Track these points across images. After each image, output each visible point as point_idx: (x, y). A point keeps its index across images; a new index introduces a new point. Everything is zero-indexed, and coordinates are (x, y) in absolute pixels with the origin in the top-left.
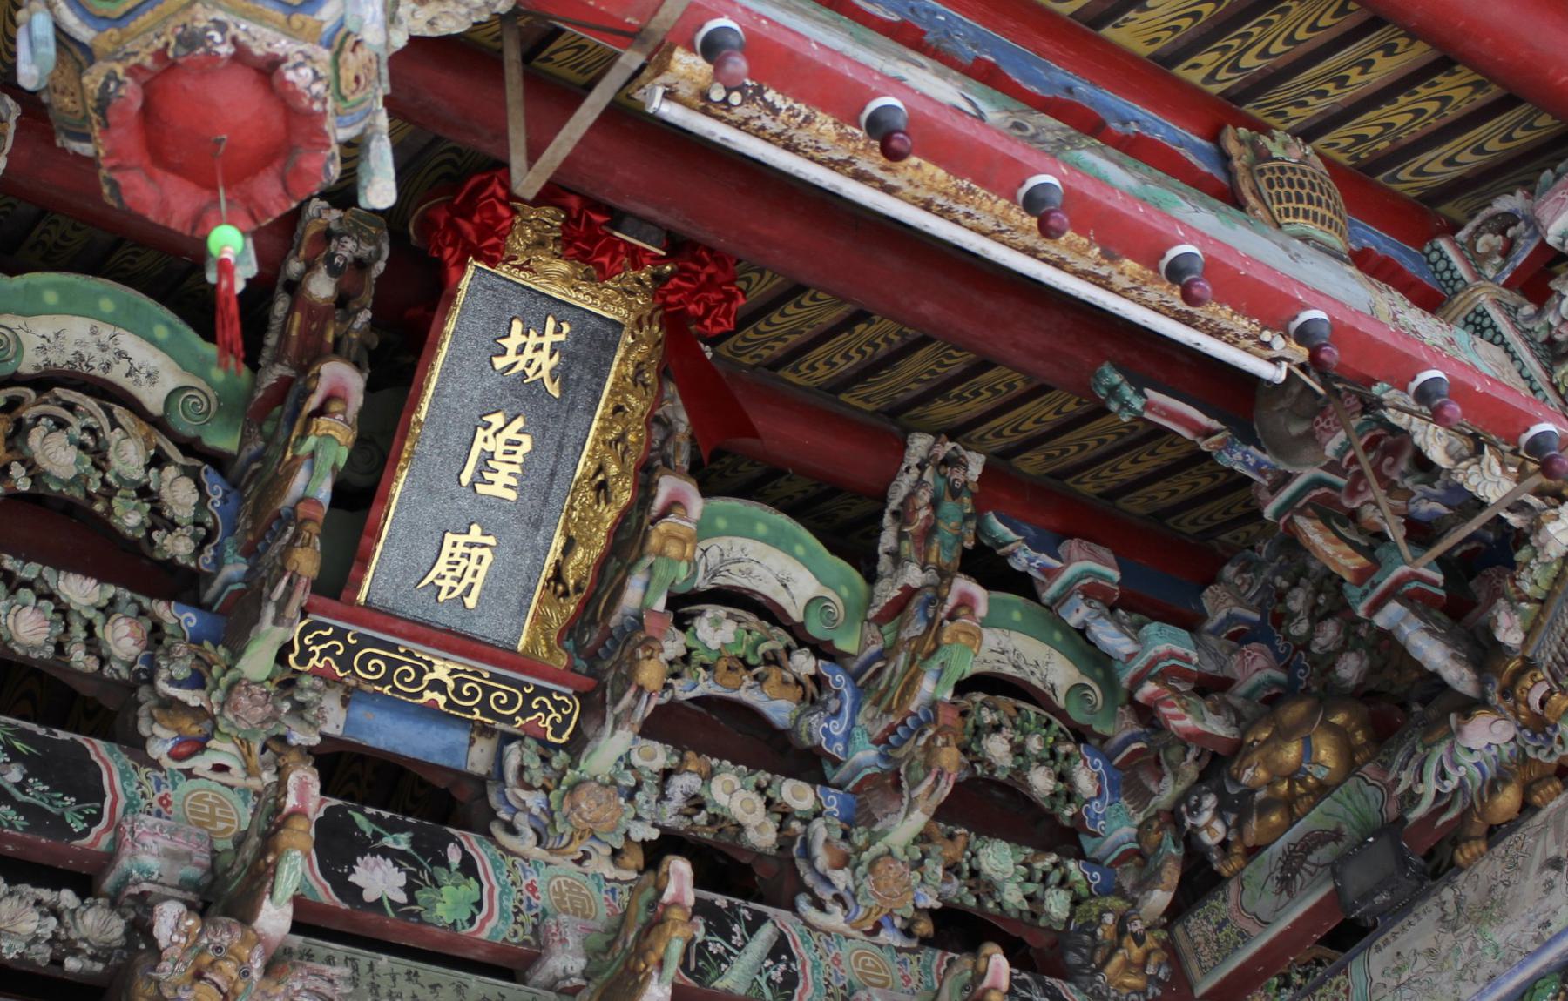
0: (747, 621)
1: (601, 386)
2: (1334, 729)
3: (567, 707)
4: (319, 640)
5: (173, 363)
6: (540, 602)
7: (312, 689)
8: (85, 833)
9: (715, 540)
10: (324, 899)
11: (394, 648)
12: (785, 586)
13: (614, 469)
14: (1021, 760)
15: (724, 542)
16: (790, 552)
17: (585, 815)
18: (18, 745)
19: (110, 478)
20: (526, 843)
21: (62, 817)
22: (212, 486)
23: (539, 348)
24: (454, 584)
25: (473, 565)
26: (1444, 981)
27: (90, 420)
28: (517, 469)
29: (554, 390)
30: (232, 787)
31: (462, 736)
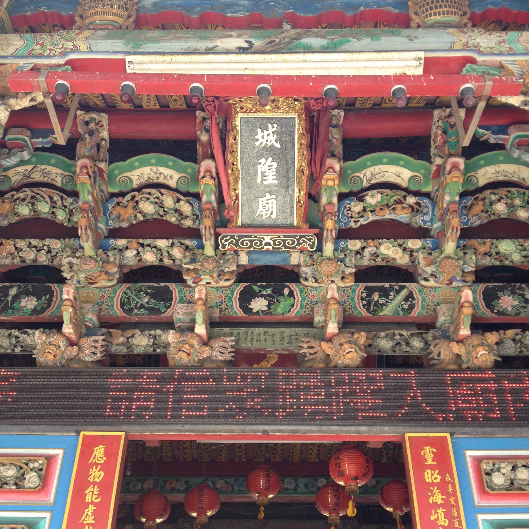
1: (294, 139)
3: (312, 239)
4: (226, 241)
7: (230, 254)
8: (166, 311)
10: (240, 315)
12: (399, 176)
13: (304, 164)
14: (512, 209)
15: (371, 169)
16: (398, 164)
18: (148, 291)
19: (166, 209)
20: (310, 283)
21: (159, 308)
23: (268, 135)
24: (267, 212)
25: (271, 205)
29: (278, 146)
30: (213, 287)
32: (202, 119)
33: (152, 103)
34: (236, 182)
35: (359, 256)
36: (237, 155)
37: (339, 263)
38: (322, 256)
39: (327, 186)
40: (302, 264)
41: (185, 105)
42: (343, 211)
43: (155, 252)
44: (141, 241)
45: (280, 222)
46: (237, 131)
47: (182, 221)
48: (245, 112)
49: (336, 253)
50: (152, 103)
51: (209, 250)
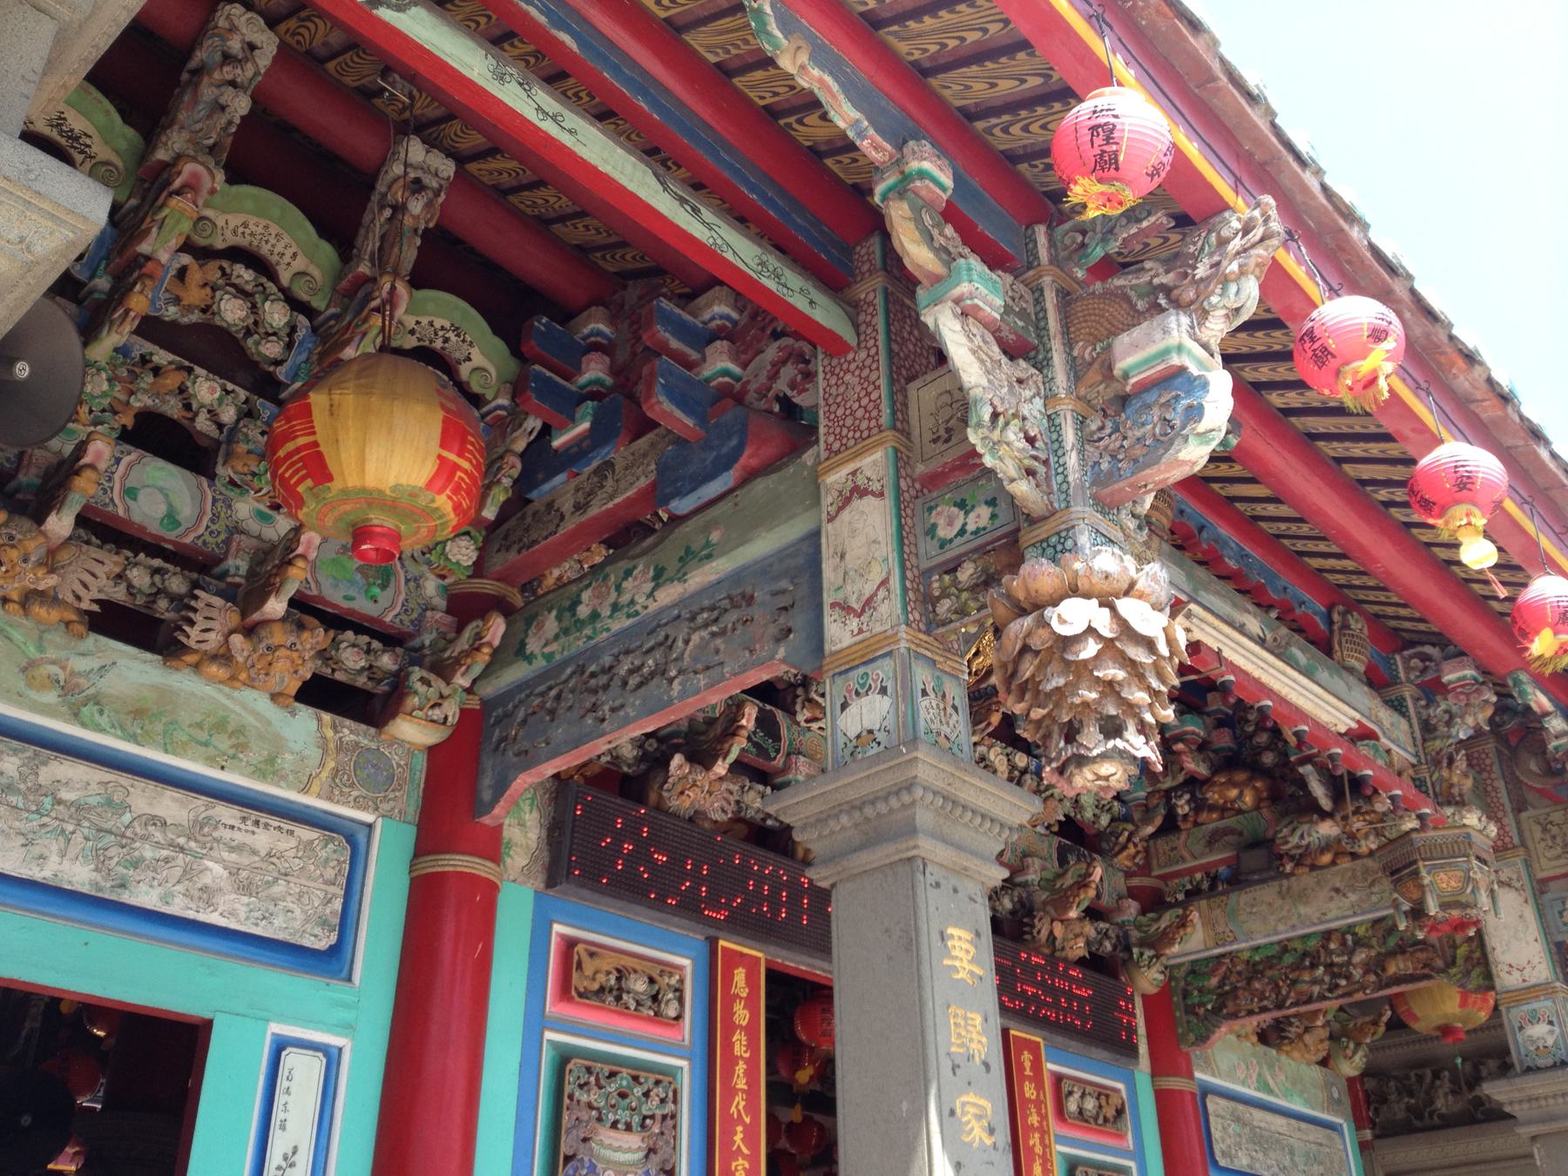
2: (1255, 788)
26: (1272, 919)
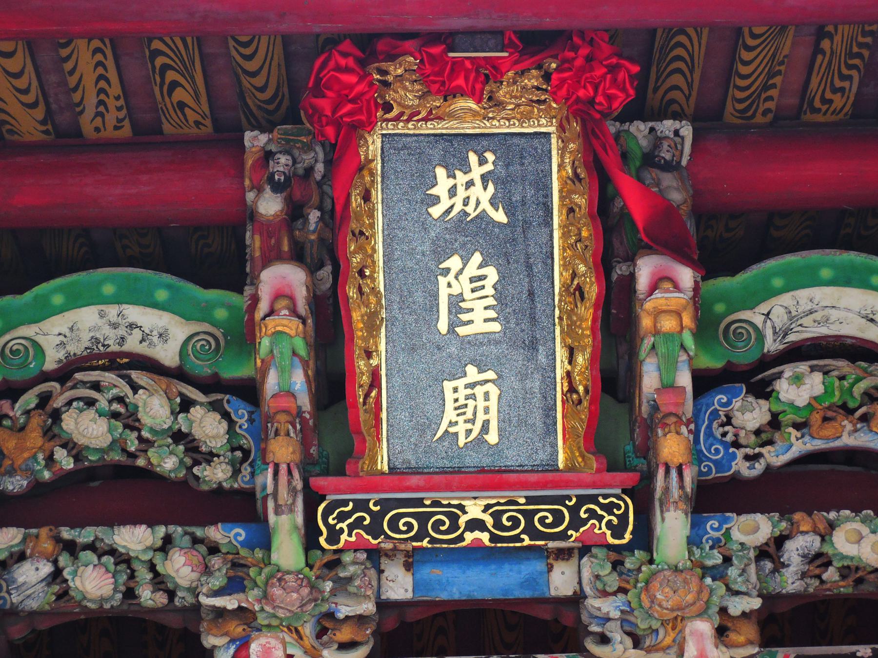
0: (837, 368)
1: (549, 196)
3: (619, 507)
4: (342, 517)
5: (177, 318)
6: (564, 417)
7: (354, 563)
9: (774, 301)
11: (419, 503)
12: (872, 320)
13: (582, 268)
15: (786, 299)
17: (664, 604)
19: (145, 434)
22: (236, 411)
23: (470, 184)
24: (469, 426)
25: (481, 404)
27: (115, 391)
28: (491, 301)
29: (500, 216)
31: (539, 566)
32: (262, 154)
33: (111, 118)
34: (372, 327)
35: (768, 565)
36: (374, 250)
37: (708, 581)
38: (651, 561)
39: (656, 332)
40: (588, 590)
41: (208, 122)
42: (709, 427)
43: (112, 567)
44: (66, 534)
45: (512, 458)
46: (372, 174)
47: (195, 470)
48: (397, 119)
49: (697, 552)
50: (111, 118)
51: (287, 550)
